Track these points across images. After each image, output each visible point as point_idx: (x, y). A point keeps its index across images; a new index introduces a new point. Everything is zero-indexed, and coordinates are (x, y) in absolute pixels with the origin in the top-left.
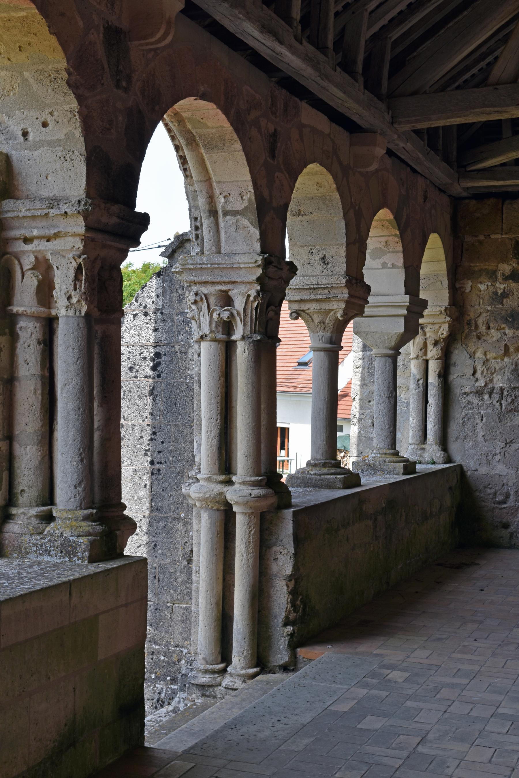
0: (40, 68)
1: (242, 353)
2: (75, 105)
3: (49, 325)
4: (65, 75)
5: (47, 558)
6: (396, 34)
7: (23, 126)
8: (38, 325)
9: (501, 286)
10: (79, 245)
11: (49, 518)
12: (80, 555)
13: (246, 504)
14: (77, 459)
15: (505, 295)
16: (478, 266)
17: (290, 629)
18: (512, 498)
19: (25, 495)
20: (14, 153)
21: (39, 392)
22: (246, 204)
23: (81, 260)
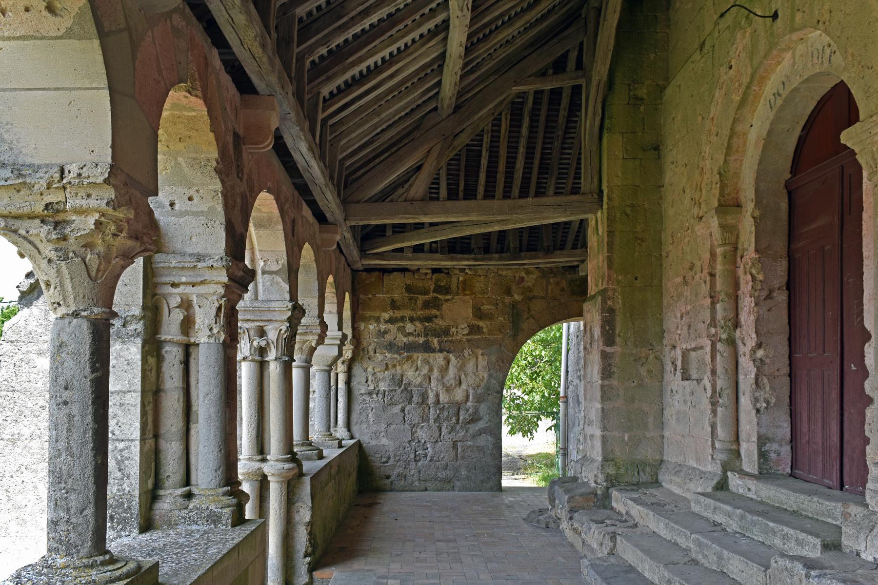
0: (194, 156)
1: (274, 369)
2: (219, 186)
3: (188, 349)
4: (215, 164)
5: (194, 527)
6: (348, 163)
7: (171, 198)
8: (180, 349)
9: (383, 327)
10: (221, 291)
11: (189, 496)
12: (224, 522)
13: (279, 475)
14: (217, 450)
15: (386, 332)
16: (368, 314)
17: (308, 559)
18: (392, 459)
19: (171, 480)
20: (161, 218)
21: (181, 400)
22: (280, 267)
23: (222, 302)
